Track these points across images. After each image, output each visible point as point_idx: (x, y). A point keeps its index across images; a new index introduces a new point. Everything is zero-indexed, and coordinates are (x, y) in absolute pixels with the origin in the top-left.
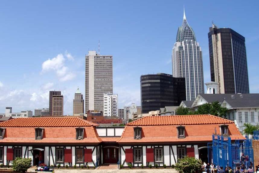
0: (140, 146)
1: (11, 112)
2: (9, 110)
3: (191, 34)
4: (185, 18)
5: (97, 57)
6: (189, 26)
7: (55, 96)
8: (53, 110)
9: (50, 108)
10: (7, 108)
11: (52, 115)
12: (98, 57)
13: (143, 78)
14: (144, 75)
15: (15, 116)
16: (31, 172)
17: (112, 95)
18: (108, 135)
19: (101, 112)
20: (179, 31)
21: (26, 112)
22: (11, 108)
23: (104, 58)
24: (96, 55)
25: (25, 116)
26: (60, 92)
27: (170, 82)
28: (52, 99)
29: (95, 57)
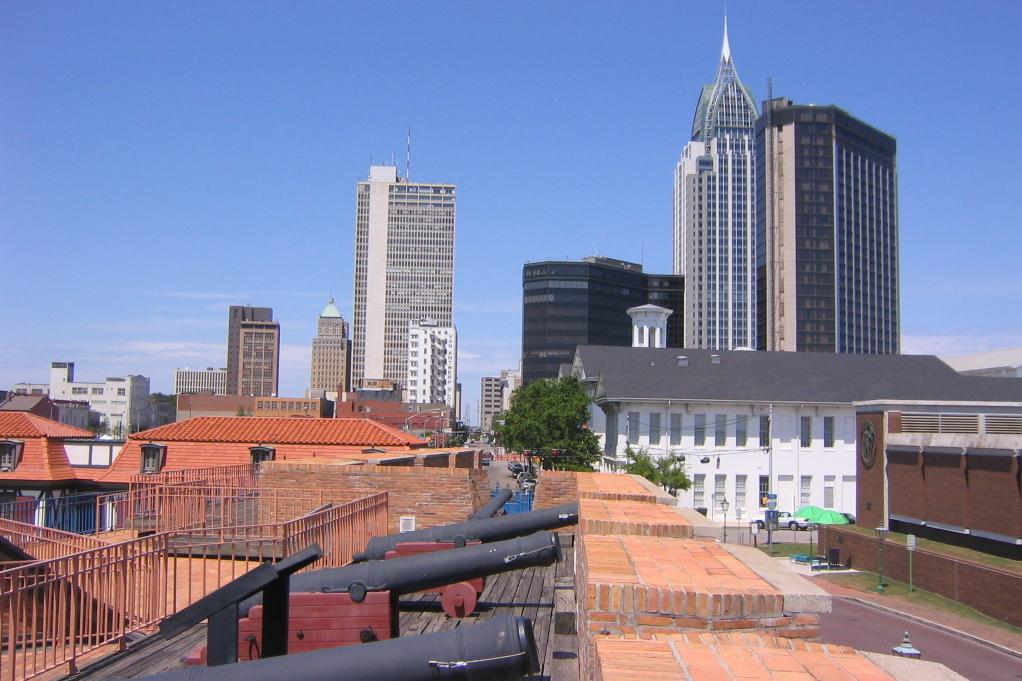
0: (10, 488)
1: (70, 379)
2: (64, 372)
3: (746, 116)
4: (726, 52)
5: (398, 191)
6: (740, 83)
7: (252, 327)
8: (240, 375)
9: (229, 366)
10: (57, 365)
11: (236, 392)
12: (401, 188)
13: (529, 273)
14: (543, 260)
15: (86, 392)
16: (838, 645)
17: (435, 329)
18: (93, 463)
19: (395, 385)
20: (702, 101)
21: (123, 380)
22: (71, 365)
23: (439, 192)
24: (397, 180)
25: (119, 393)
26: (269, 312)
27: (626, 292)
28: (238, 334)
29: (391, 188)
